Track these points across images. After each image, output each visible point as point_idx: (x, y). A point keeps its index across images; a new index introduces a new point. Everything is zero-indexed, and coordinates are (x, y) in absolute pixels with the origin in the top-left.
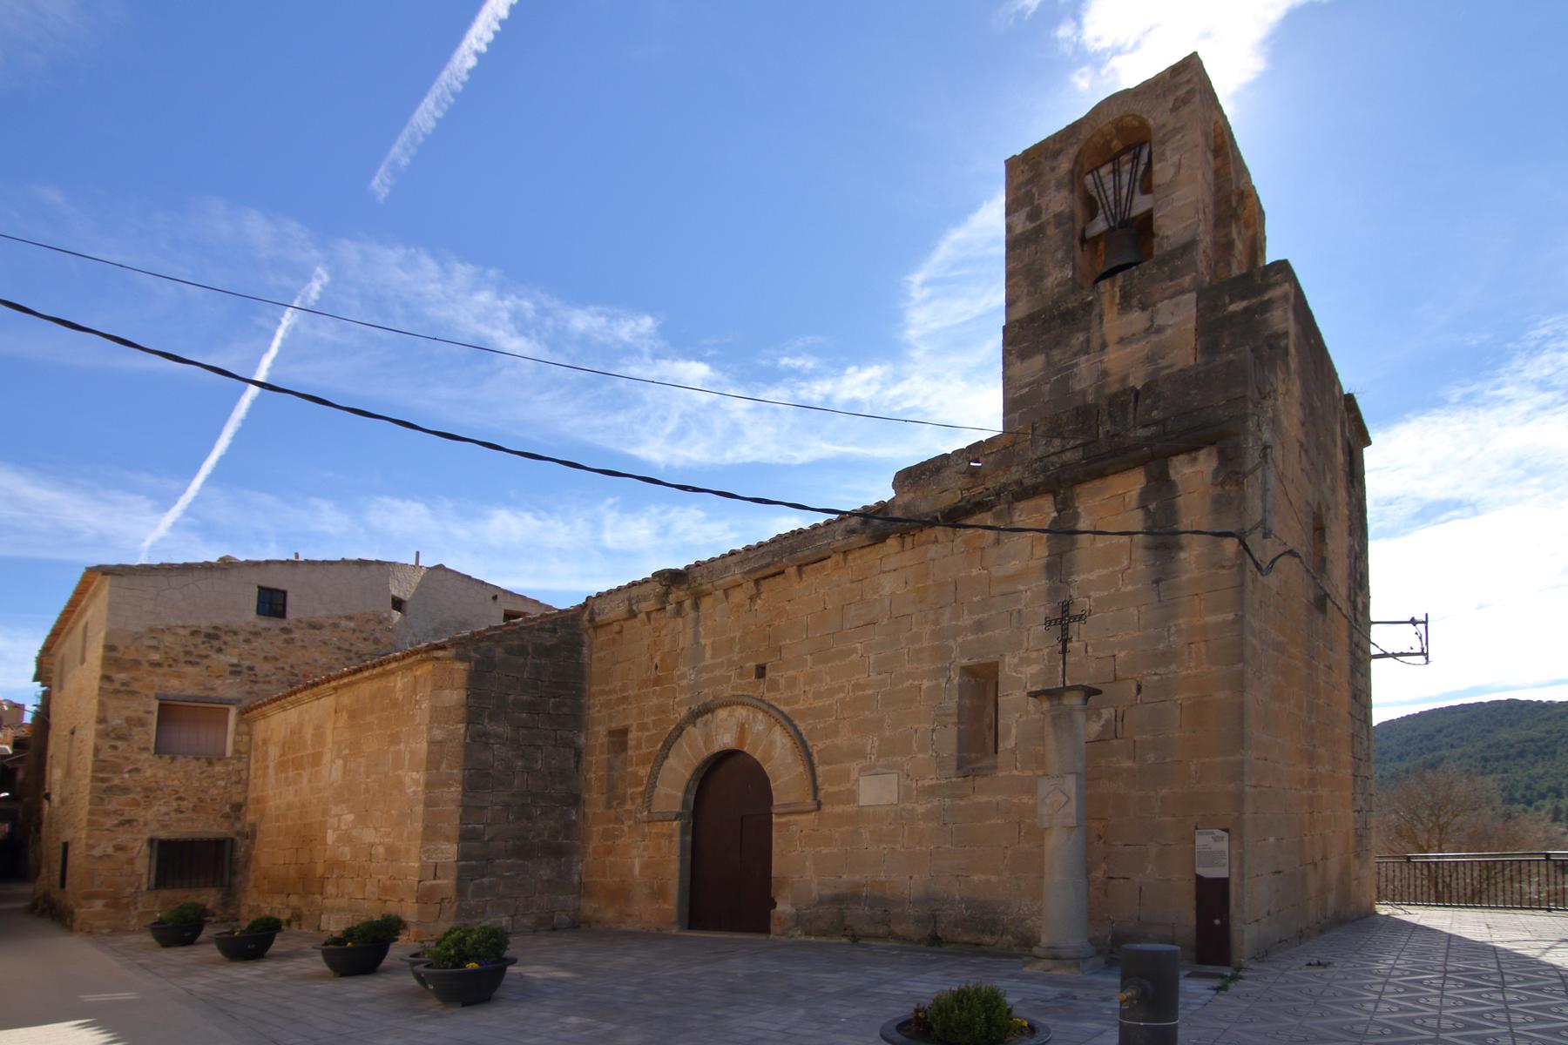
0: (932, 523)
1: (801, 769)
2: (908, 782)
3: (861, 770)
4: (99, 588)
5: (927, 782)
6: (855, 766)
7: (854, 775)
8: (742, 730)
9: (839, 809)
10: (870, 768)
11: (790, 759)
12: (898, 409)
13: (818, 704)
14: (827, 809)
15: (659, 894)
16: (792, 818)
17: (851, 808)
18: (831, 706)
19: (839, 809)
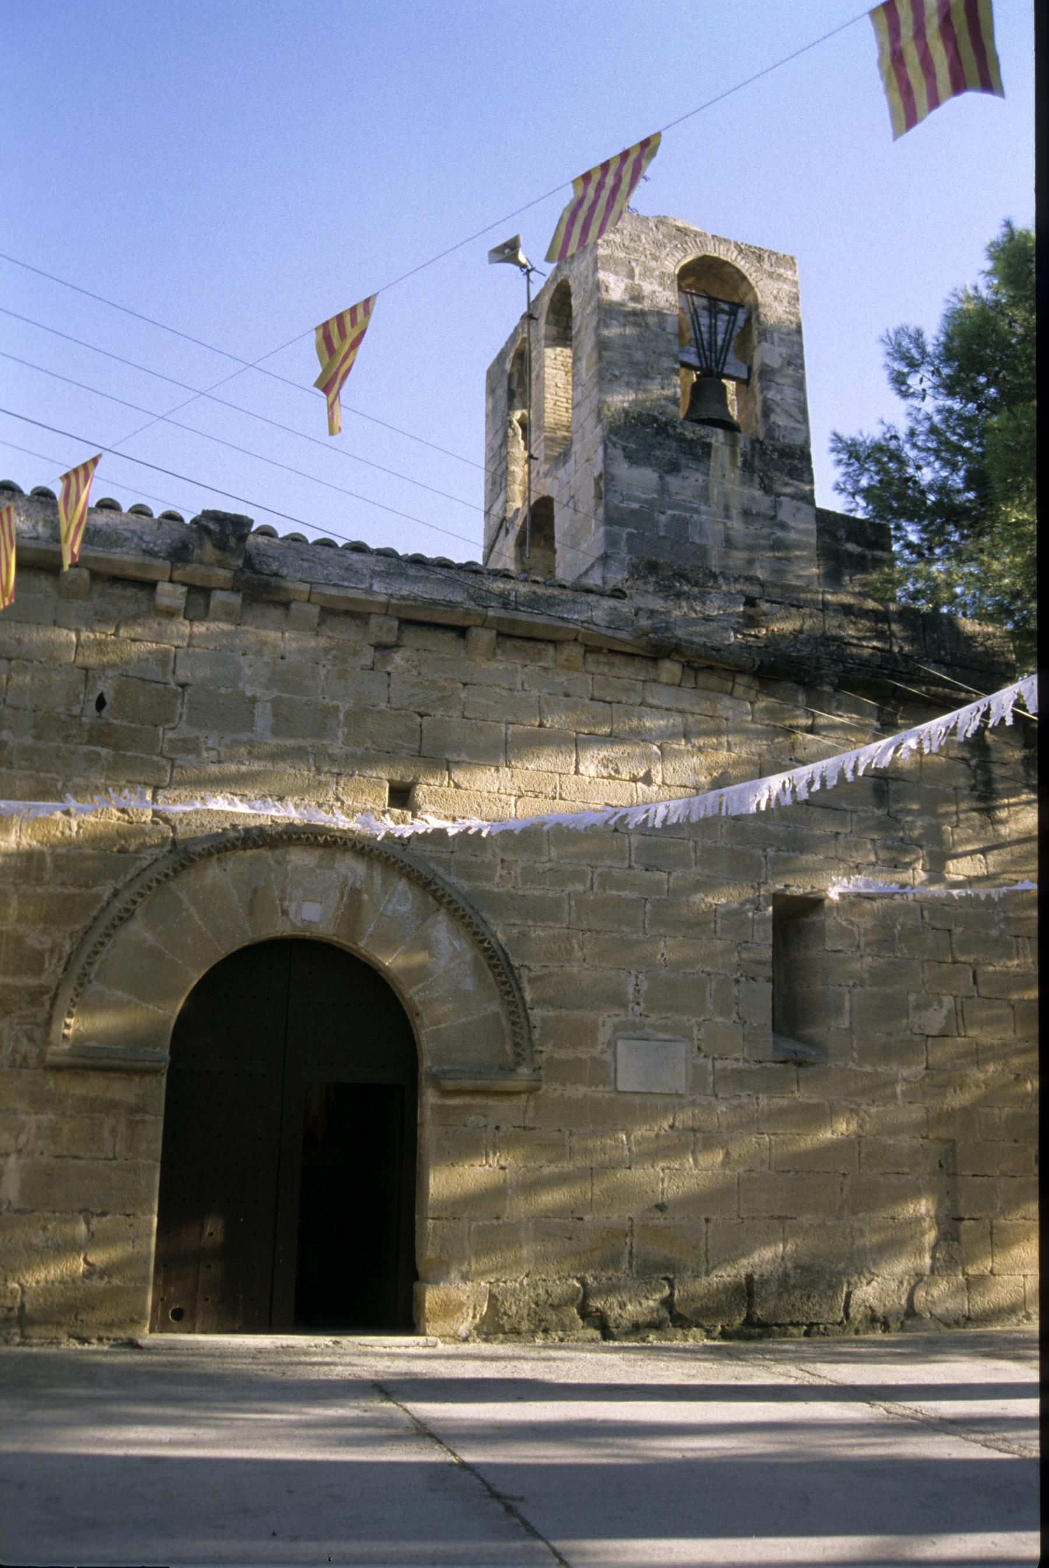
0: (735, 670)
1: (494, 1007)
2: (701, 1060)
3: (616, 1028)
4: (55, 1054)
5: (730, 1064)
6: (607, 1020)
7: (604, 1035)
8: (353, 903)
9: (579, 1091)
10: (634, 1026)
11: (469, 984)
12: (464, 885)
13: (536, 892)
14: (551, 1090)
15: (1000, 855)
16: (478, 1101)
17: (600, 1092)
18: (557, 903)
19: (579, 1091)
